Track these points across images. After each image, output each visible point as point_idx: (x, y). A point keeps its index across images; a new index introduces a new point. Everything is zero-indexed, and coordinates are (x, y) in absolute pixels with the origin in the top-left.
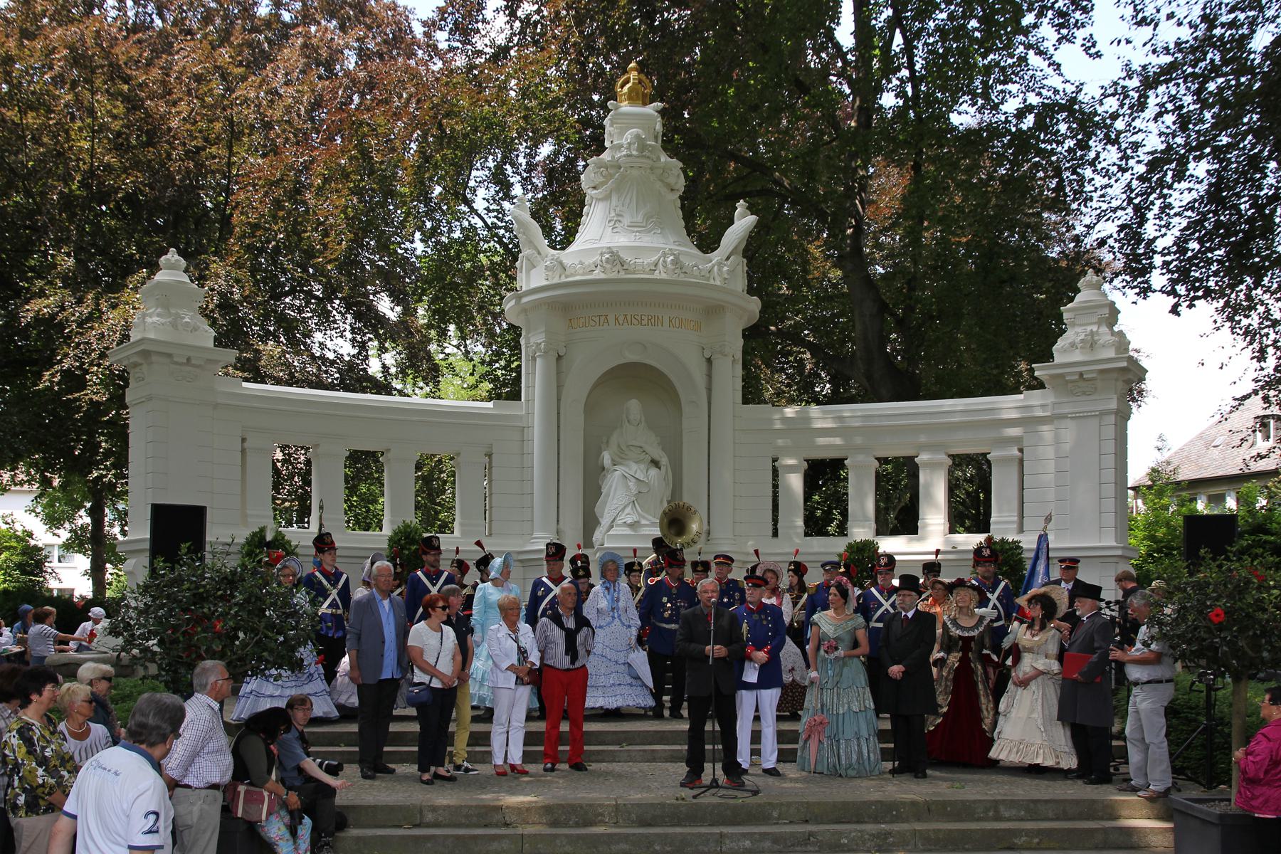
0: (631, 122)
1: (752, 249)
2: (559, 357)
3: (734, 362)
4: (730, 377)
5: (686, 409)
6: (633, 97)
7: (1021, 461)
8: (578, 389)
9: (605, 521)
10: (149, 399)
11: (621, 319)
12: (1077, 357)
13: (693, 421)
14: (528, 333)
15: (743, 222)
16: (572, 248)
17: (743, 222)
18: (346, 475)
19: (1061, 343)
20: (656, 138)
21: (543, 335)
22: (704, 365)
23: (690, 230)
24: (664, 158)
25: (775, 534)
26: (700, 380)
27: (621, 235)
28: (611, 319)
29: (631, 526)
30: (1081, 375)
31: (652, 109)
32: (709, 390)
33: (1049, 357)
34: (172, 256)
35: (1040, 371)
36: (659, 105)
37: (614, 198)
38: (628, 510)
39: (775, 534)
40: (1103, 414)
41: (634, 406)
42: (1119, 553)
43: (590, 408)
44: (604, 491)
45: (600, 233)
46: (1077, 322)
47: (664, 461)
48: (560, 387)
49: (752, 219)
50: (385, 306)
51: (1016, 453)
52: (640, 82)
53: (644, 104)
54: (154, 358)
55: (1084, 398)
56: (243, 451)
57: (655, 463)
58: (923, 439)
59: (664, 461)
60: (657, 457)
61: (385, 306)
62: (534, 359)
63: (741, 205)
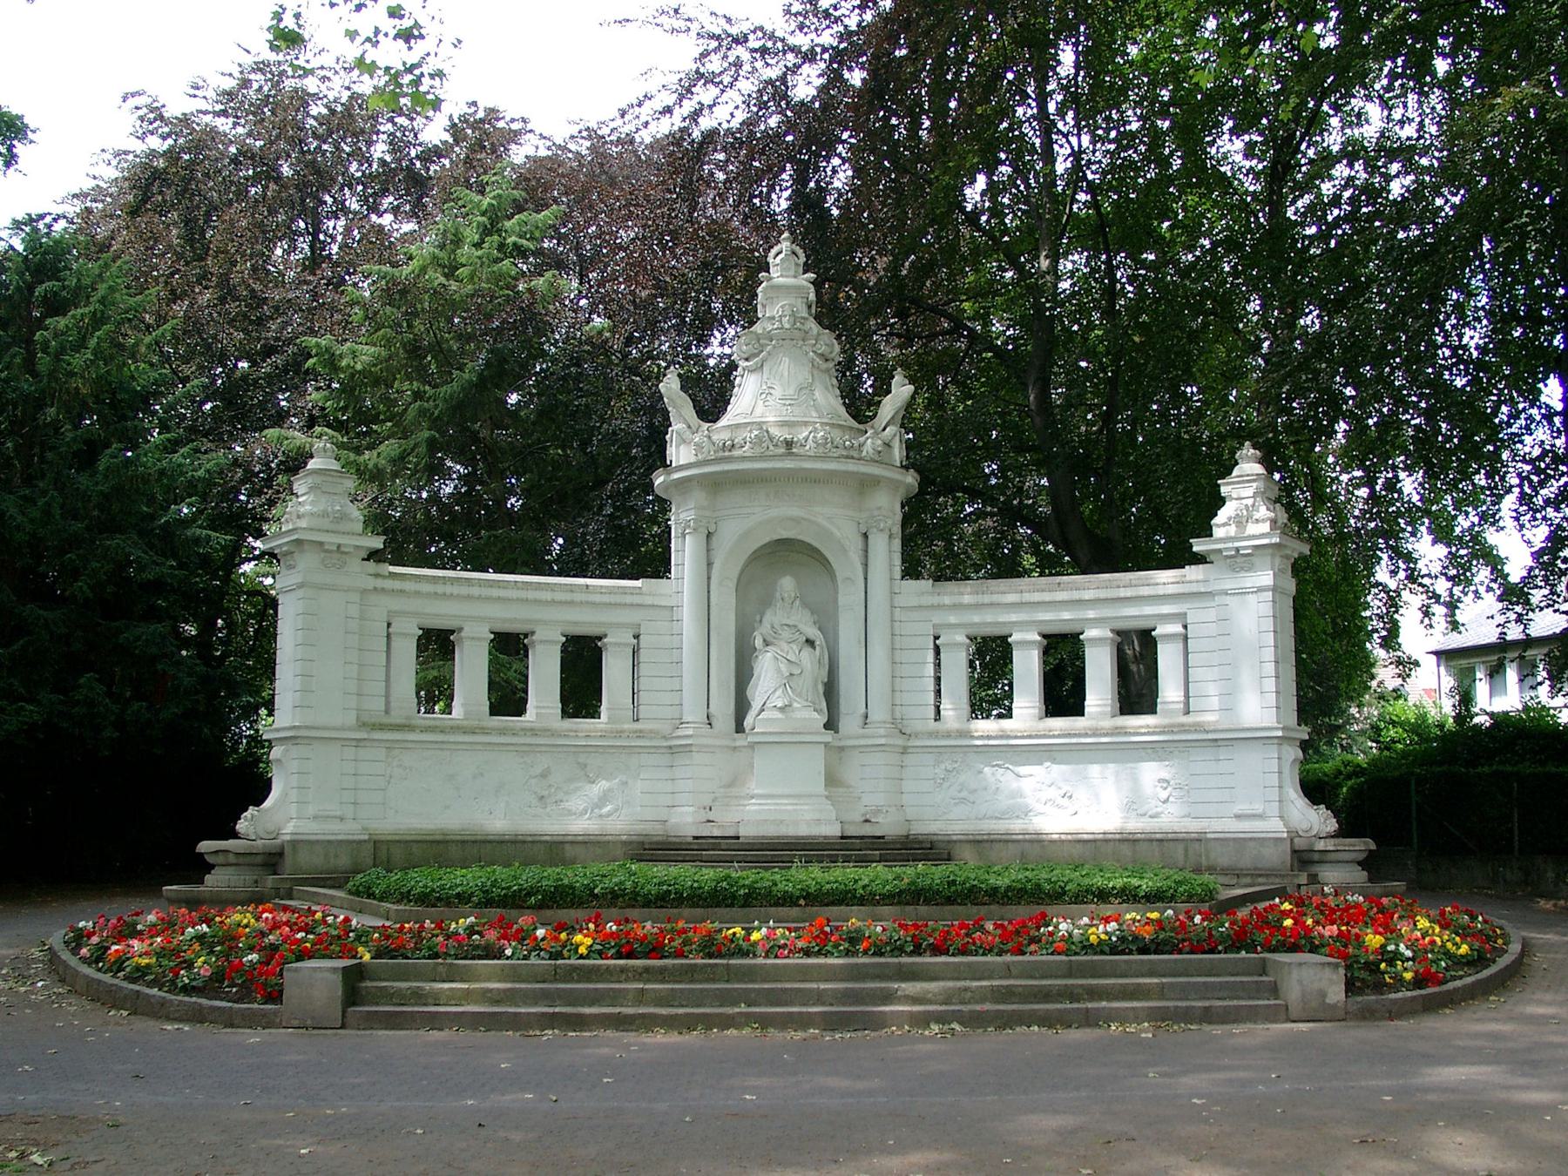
2: (709, 535)
4: (886, 552)
5: (840, 575)
7: (1186, 638)
8: (727, 571)
9: (756, 705)
13: (849, 597)
16: (723, 422)
19: (1223, 514)
29: (782, 709)
30: (1237, 550)
33: (1207, 532)
35: (1198, 546)
36: (812, 275)
38: (779, 692)
41: (787, 584)
42: (1280, 734)
43: (743, 585)
47: (819, 639)
48: (710, 564)
54: (306, 547)
56: (388, 636)
57: (810, 643)
58: (1091, 614)
59: (819, 639)
60: (812, 637)
62: (684, 536)
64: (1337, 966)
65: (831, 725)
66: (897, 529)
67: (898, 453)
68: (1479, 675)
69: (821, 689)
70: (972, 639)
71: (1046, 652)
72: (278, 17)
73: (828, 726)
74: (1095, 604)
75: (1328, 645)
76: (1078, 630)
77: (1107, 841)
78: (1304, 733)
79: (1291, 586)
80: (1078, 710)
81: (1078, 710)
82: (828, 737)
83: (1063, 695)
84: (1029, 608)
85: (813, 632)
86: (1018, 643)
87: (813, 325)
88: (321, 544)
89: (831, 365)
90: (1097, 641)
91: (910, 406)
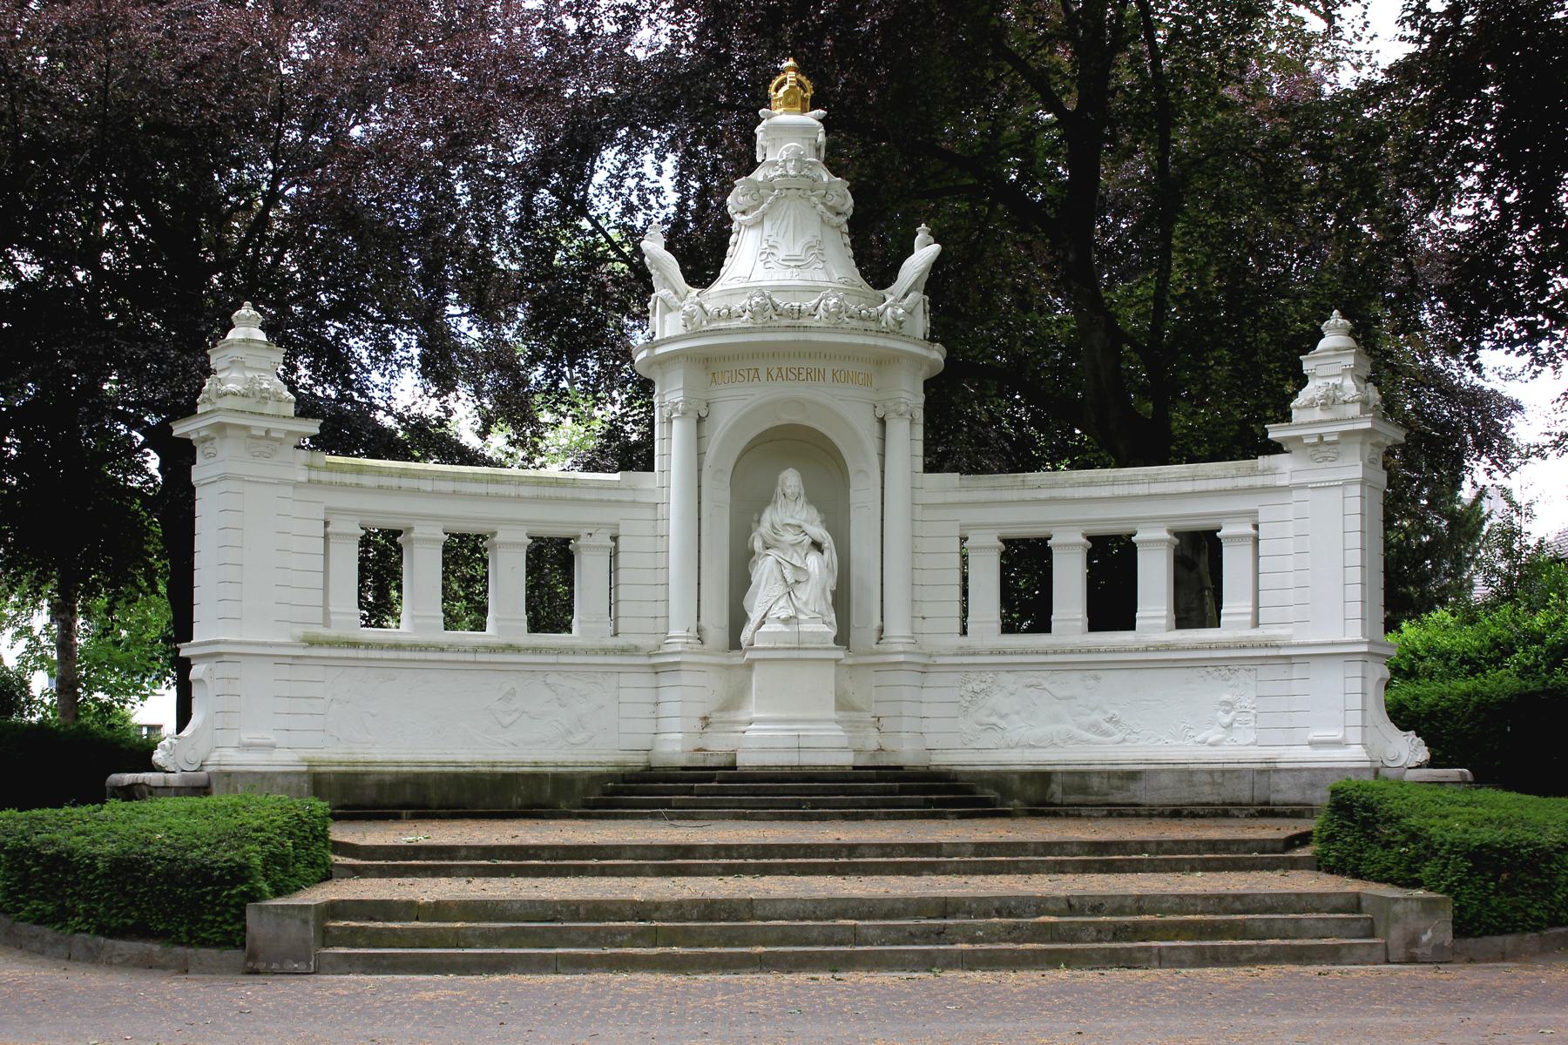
0: (788, 131)
1: (935, 282)
3: (912, 421)
4: (907, 441)
6: (789, 104)
7: (1256, 540)
9: (755, 617)
10: (224, 477)
11: (774, 373)
12: (1317, 414)
13: (862, 495)
14: (662, 389)
15: (924, 253)
16: (716, 287)
17: (924, 253)
18: (1070, 467)
20: (818, 150)
21: (681, 393)
22: (877, 426)
23: (860, 258)
24: (826, 176)
25: (964, 632)
26: (872, 448)
27: (782, 255)
28: (763, 375)
30: (1321, 437)
31: (812, 118)
32: (883, 455)
33: (1286, 417)
34: (247, 310)
35: (1275, 433)
37: (767, 224)
38: (782, 603)
39: (964, 632)
40: (1347, 483)
42: (1365, 648)
44: (754, 580)
45: (758, 261)
46: (1318, 373)
48: (700, 454)
49: (936, 248)
50: (467, 330)
51: (1252, 531)
52: (800, 84)
53: (804, 111)
54: (229, 432)
55: (1327, 464)
56: (326, 537)
57: (817, 546)
59: (828, 542)
60: (819, 539)
61: (467, 330)
62: (670, 421)
63: (922, 232)
91: (938, 264)
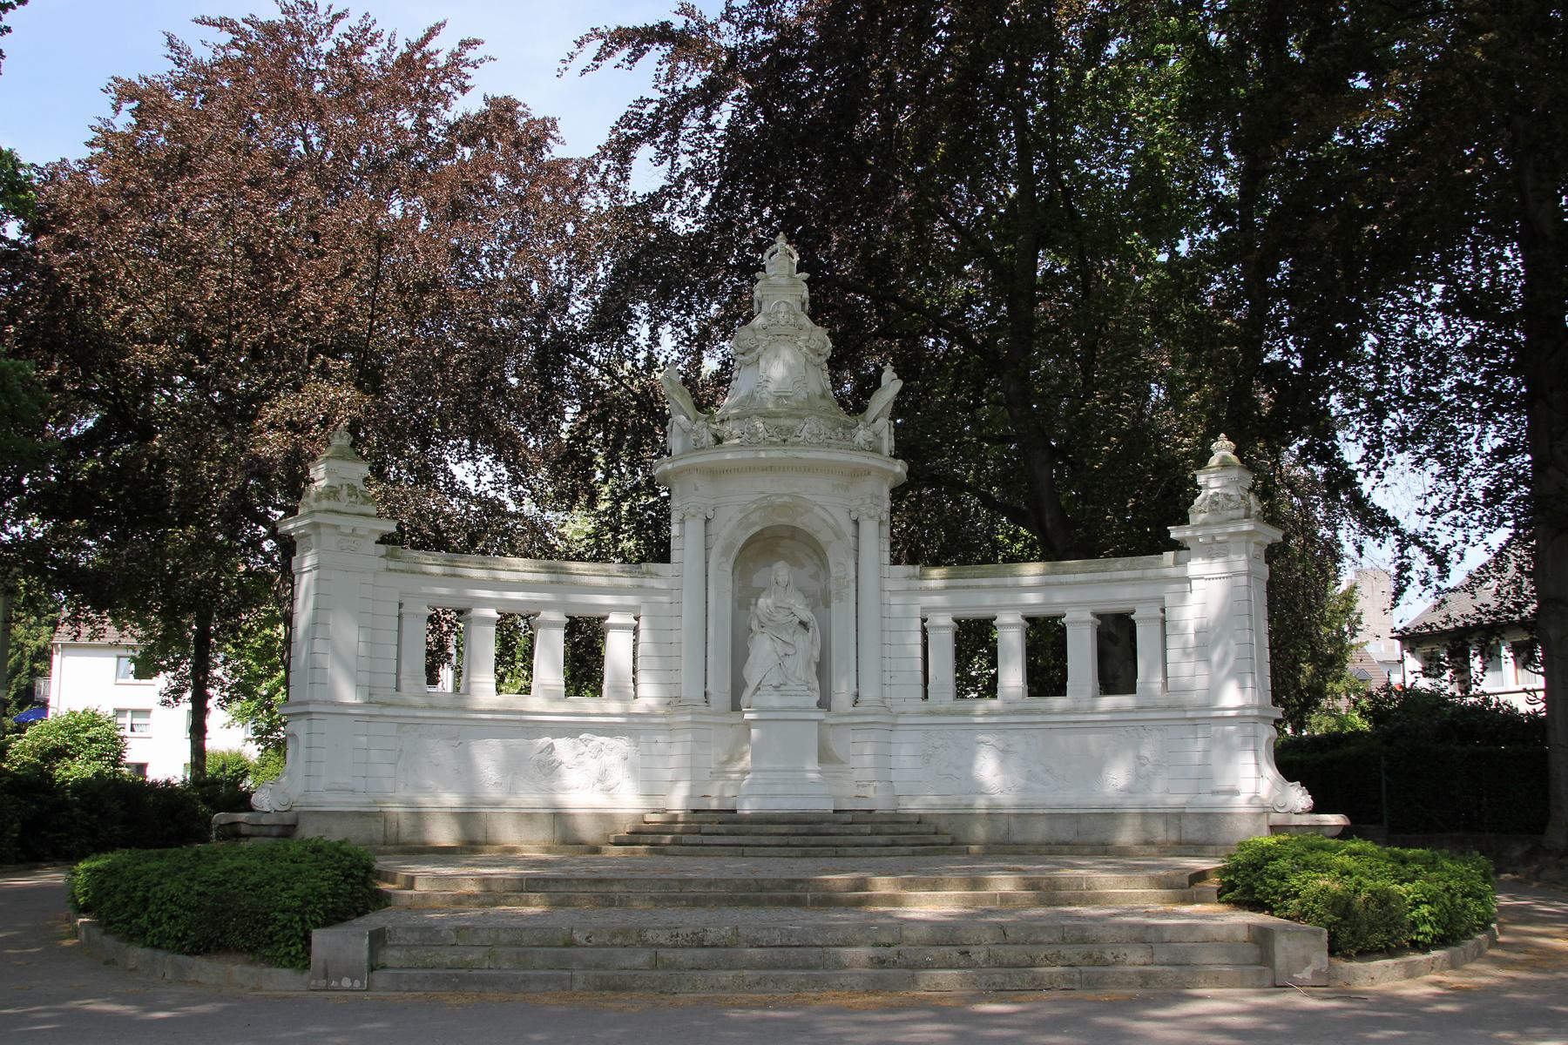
0: (781, 280)
2: (707, 521)
4: (875, 543)
9: (752, 685)
35: (1175, 533)
42: (1256, 712)
54: (322, 530)
56: (400, 617)
60: (805, 619)
64: (1317, 934)
65: (824, 704)
66: (886, 516)
67: (888, 443)
68: (1504, 652)
69: (814, 668)
70: (957, 621)
71: (569, 635)
72: (432, 33)
73: (819, 705)
74: (1077, 593)
75: (1298, 624)
76: (603, 614)
77: (19, 861)
78: (1278, 712)
79: (1265, 570)
80: (1130, 689)
81: (1061, 690)
82: (821, 715)
83: (1046, 675)
84: (1024, 590)
85: (806, 615)
86: (1075, 622)
87: (806, 321)
88: (336, 527)
89: (824, 359)
90: (1146, 619)
